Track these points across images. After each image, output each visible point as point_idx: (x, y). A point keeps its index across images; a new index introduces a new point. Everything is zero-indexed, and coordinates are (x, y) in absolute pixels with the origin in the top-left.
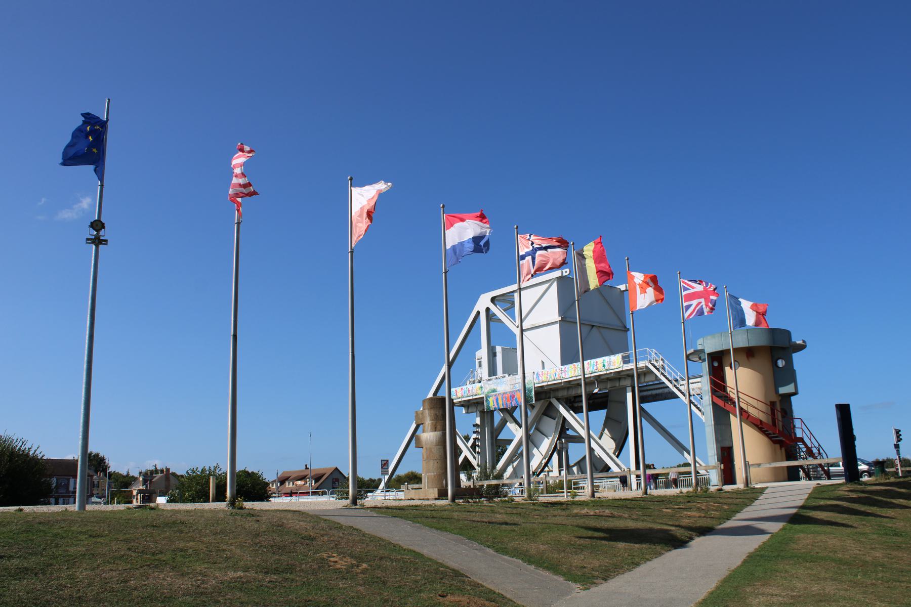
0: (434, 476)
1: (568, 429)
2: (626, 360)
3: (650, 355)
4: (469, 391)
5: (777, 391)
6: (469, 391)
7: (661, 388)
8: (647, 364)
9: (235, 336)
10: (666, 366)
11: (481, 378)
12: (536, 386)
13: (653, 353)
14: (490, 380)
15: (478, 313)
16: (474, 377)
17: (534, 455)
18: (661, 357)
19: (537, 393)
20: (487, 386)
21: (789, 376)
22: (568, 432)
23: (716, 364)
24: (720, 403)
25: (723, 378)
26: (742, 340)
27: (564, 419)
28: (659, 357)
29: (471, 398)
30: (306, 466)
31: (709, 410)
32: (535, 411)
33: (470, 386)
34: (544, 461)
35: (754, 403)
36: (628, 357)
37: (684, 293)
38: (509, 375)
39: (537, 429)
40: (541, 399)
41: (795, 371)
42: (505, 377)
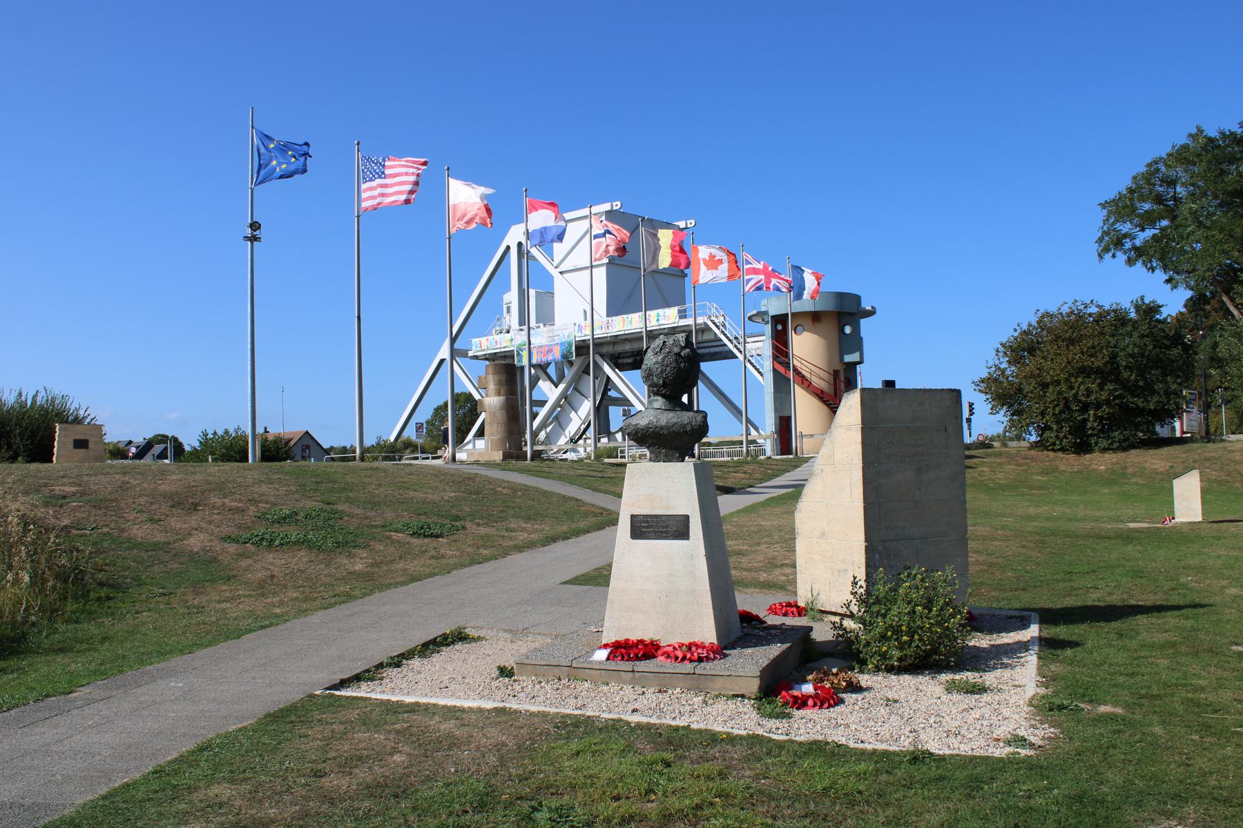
0: (498, 439)
1: (610, 390)
2: (682, 314)
3: (710, 310)
4: (496, 342)
5: (842, 359)
6: (496, 342)
7: (718, 346)
8: (706, 321)
9: (359, 318)
10: (727, 324)
11: (510, 327)
12: (577, 339)
13: (713, 308)
14: (521, 330)
15: (508, 248)
16: (500, 325)
17: (571, 420)
18: (722, 313)
19: (577, 348)
20: (518, 337)
21: (855, 343)
22: (610, 393)
23: (780, 327)
24: (781, 369)
25: (786, 344)
26: (806, 304)
27: (608, 378)
28: (720, 313)
29: (498, 351)
30: (266, 428)
31: (769, 376)
32: (574, 368)
33: (498, 338)
34: (583, 427)
35: (817, 370)
36: (685, 311)
37: (746, 267)
38: (545, 325)
39: (576, 389)
40: (581, 355)
41: (862, 338)
42: (539, 327)
